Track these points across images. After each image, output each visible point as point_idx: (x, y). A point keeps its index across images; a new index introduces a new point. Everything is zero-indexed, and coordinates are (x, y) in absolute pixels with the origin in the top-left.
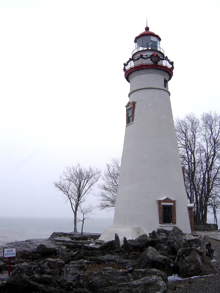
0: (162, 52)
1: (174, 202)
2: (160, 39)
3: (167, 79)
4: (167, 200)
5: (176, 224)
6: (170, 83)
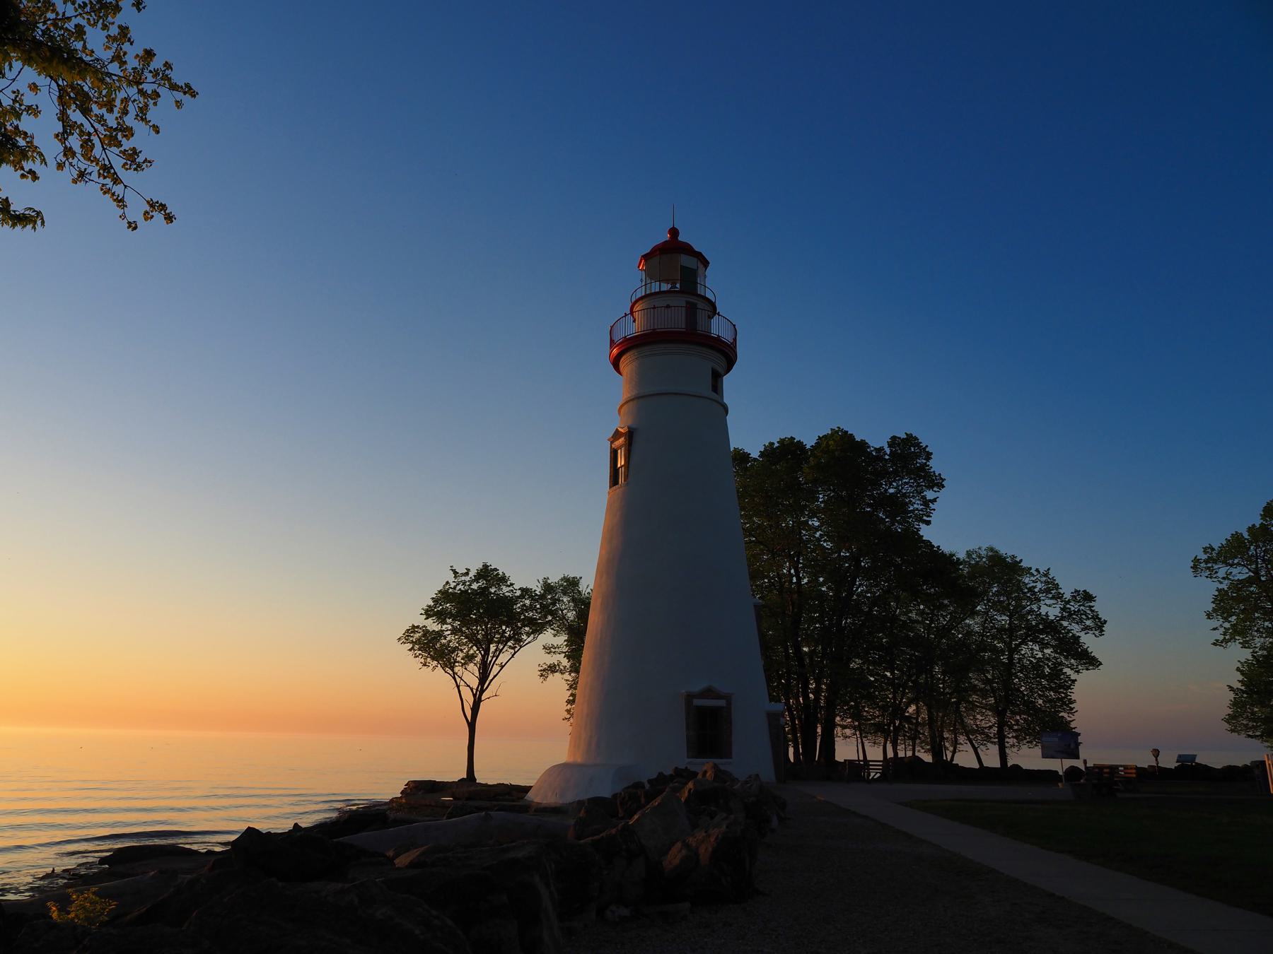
0: (712, 298)
1: (728, 698)
2: (706, 263)
3: (720, 370)
4: (708, 693)
5: (731, 758)
6: (727, 380)
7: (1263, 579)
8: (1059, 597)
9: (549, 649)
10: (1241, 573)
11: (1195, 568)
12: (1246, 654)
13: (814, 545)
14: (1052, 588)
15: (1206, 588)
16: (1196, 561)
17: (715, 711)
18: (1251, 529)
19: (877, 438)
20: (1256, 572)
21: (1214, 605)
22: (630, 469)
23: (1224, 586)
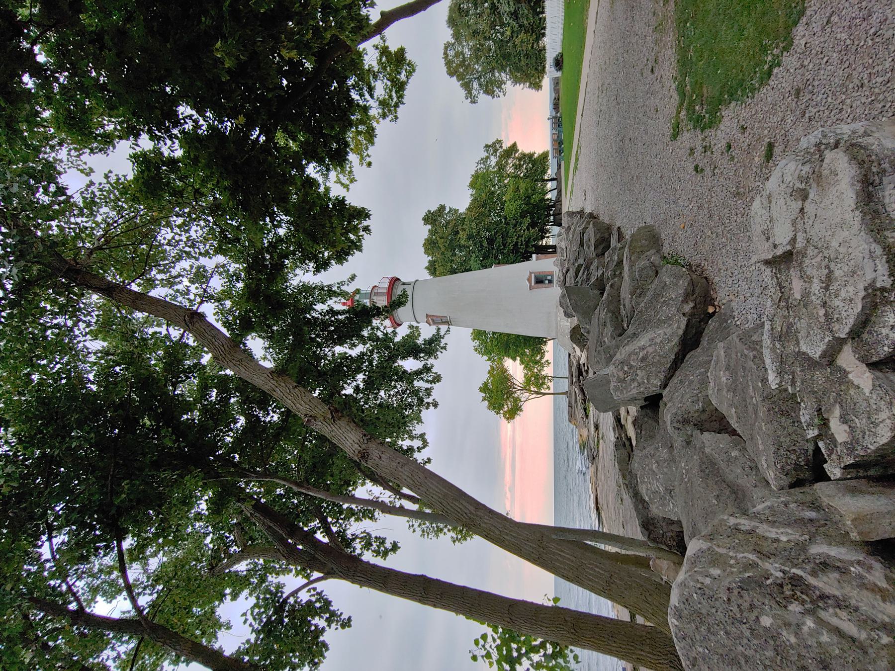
1: (531, 273)
4: (529, 280)
7: (480, 69)
8: (487, 158)
9: (66, 148)
10: (475, 85)
11: (474, 102)
12: (509, 83)
13: (34, 474)
14: (485, 160)
15: (483, 98)
16: (471, 102)
17: (536, 278)
18: (459, 81)
19: (424, 231)
20: (475, 79)
21: (429, 227)
22: (603, 514)
23: (482, 92)
